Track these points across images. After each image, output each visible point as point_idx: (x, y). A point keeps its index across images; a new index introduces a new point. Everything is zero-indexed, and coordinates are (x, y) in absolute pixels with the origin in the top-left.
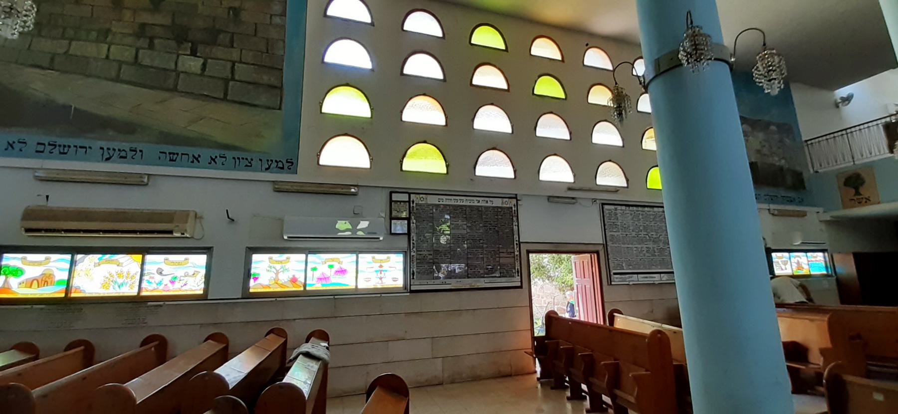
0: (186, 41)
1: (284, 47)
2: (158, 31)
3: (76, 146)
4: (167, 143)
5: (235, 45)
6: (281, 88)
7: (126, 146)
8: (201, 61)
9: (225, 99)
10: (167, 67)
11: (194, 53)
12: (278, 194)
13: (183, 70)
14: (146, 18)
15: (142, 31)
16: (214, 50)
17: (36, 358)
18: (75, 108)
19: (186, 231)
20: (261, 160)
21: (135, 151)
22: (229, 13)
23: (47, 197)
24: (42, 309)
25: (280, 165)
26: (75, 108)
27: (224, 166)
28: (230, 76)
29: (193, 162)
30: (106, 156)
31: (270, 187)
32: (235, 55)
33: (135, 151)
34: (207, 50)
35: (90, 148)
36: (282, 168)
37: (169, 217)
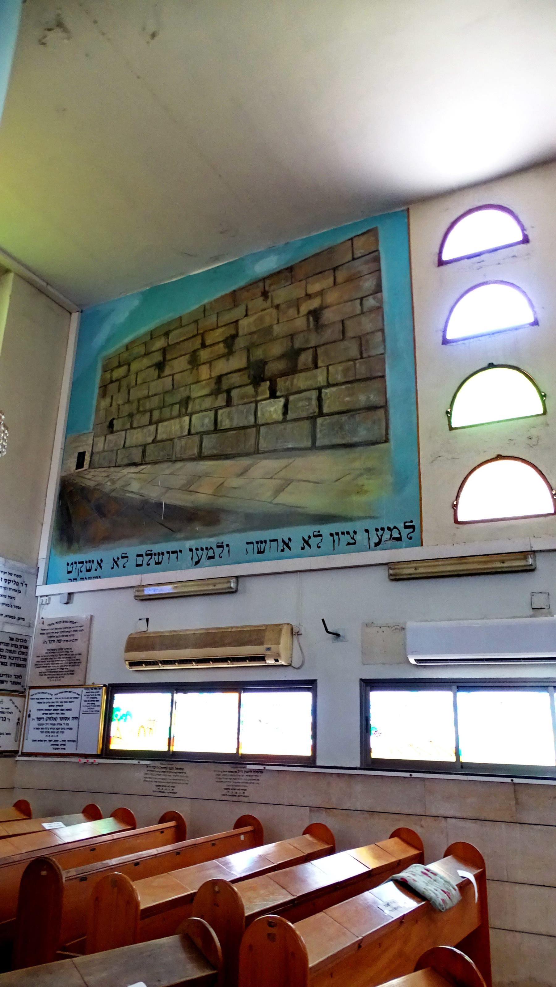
0: (264, 380)
1: (384, 340)
2: (236, 379)
3: (168, 552)
4: (253, 529)
5: (320, 364)
6: (385, 407)
7: (212, 541)
8: (282, 401)
9: (314, 447)
10: (246, 424)
11: (273, 395)
12: (395, 583)
13: (264, 421)
14: (221, 367)
15: (220, 387)
16: (295, 381)
17: (134, 828)
18: (166, 504)
19: (279, 655)
20: (367, 531)
21: (222, 546)
22: (308, 319)
23: (147, 620)
24: (147, 766)
25: (396, 534)
26: (166, 504)
27: (320, 551)
28: (317, 410)
29: (303, 548)
30: (196, 559)
31: (383, 573)
32: (320, 378)
33: (222, 546)
34: (288, 383)
35: (181, 551)
36: (399, 539)
37: (255, 635)
